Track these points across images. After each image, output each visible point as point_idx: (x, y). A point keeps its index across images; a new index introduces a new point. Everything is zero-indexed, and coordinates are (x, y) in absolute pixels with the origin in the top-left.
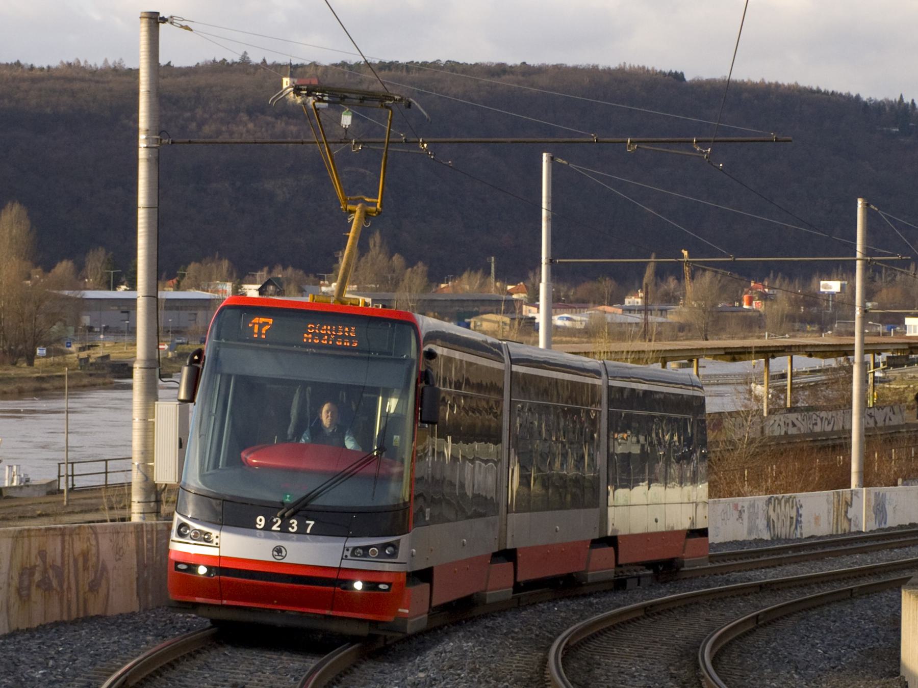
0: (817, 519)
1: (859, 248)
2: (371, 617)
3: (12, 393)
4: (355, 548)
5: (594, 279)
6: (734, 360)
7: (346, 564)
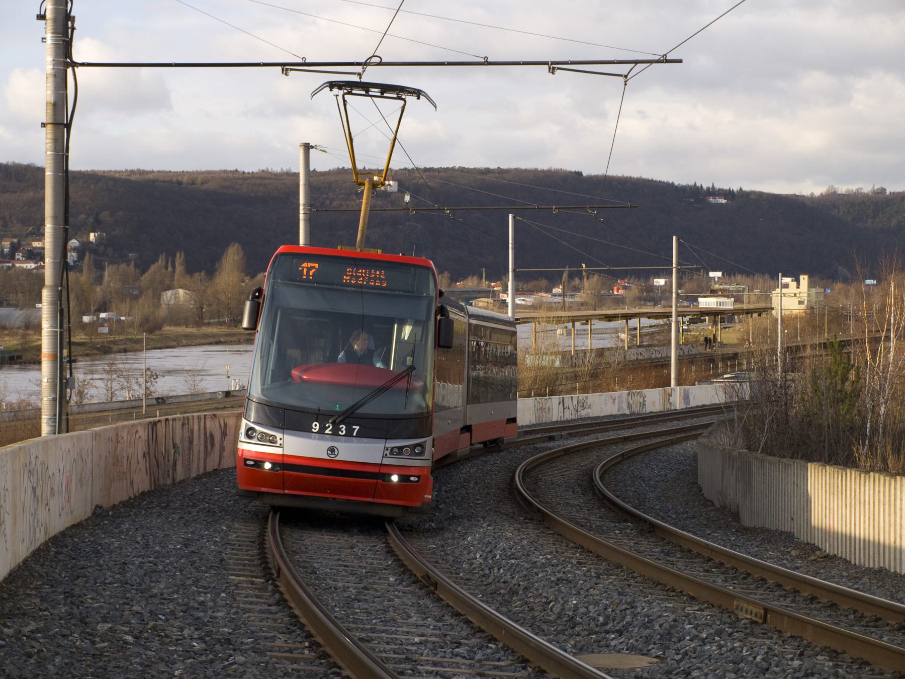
0: (654, 403)
1: (674, 262)
2: (401, 503)
3: (235, 341)
4: (393, 448)
5: (537, 279)
6: (610, 321)
7: (386, 461)
